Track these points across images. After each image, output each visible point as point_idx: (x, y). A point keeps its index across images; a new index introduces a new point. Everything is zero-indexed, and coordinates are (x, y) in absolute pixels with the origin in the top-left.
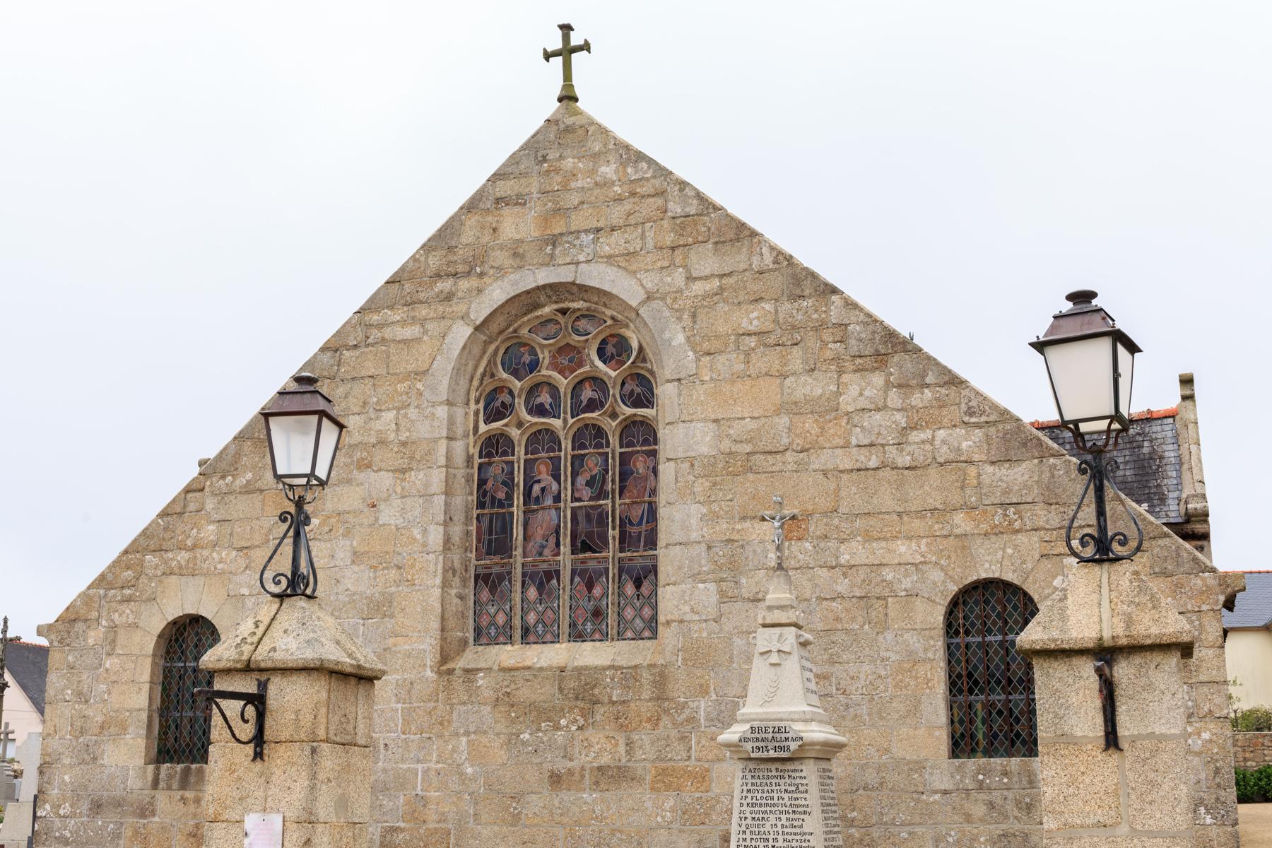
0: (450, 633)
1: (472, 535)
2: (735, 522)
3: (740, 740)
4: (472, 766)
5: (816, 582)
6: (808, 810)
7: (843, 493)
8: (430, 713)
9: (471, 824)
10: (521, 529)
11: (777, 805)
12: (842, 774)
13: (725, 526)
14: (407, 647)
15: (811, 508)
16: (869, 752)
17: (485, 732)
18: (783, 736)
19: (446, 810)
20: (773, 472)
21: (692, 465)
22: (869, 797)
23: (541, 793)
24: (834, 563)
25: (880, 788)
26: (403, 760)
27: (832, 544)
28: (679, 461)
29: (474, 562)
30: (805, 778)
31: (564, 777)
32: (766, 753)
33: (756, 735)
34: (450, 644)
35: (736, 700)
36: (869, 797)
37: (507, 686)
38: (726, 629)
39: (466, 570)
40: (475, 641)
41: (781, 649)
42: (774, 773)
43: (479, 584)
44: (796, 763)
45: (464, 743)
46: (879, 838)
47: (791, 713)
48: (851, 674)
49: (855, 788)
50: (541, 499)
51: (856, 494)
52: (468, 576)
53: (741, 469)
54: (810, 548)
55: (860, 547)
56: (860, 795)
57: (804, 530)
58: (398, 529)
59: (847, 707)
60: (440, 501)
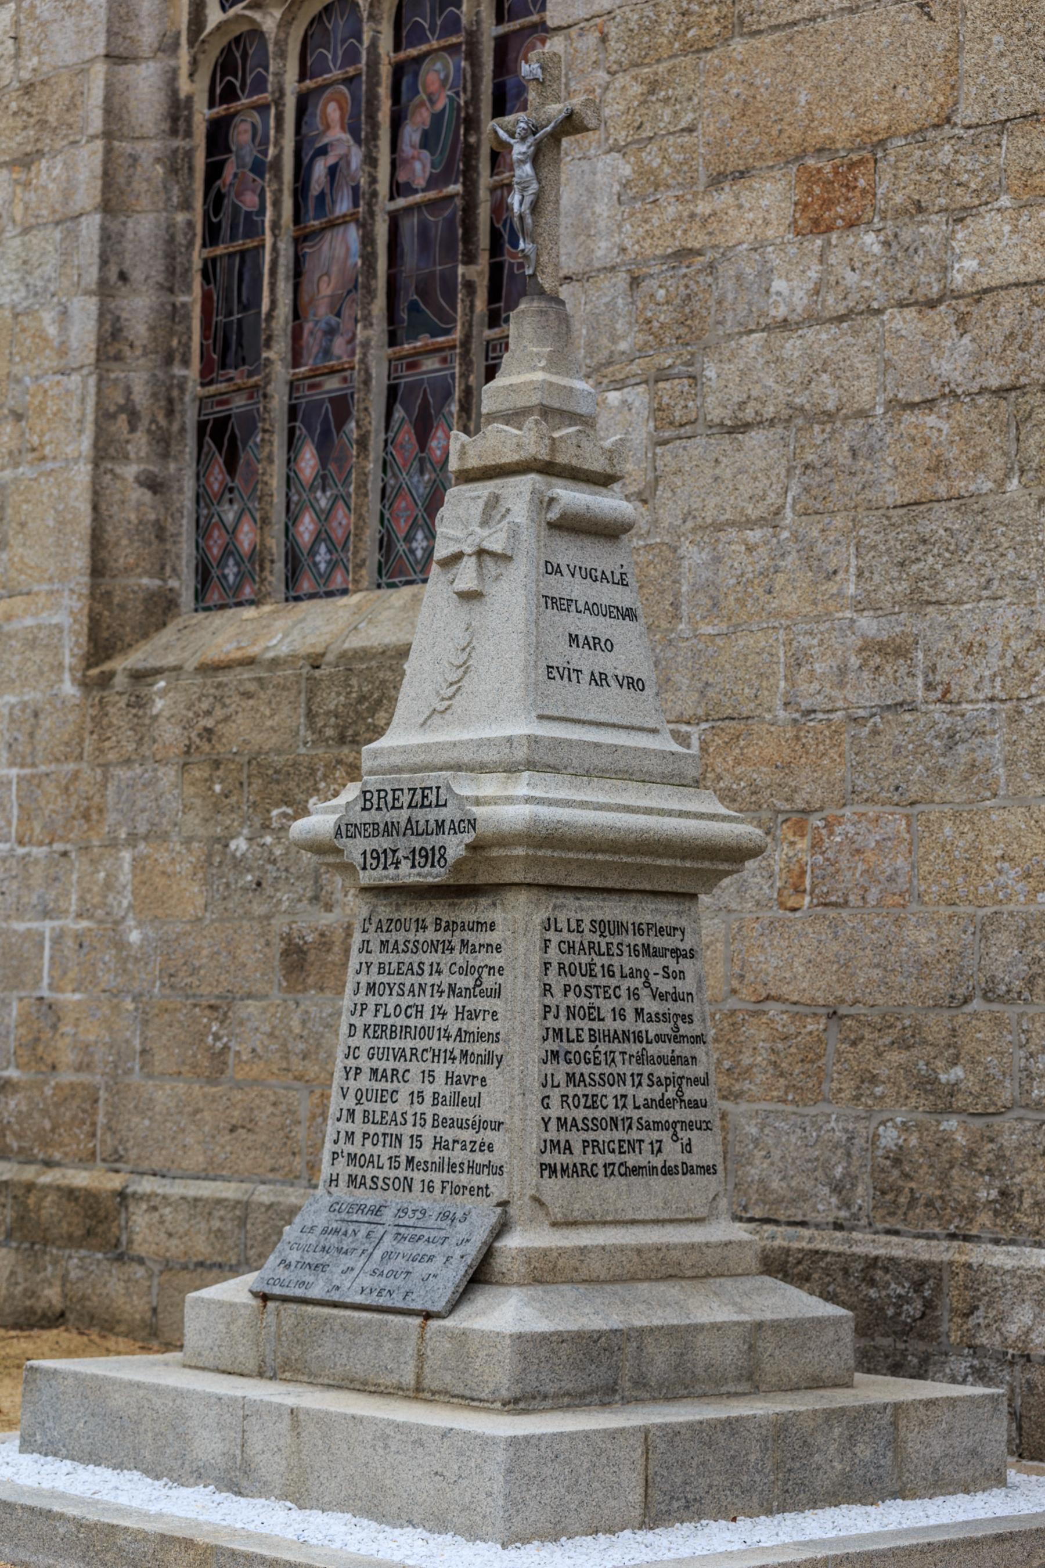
0: (122, 581)
1: (187, 317)
2: (695, 195)
3: (338, 833)
4: (140, 924)
5: (887, 353)
6: (498, 1049)
7: (967, 62)
8: (67, 789)
9: (136, 1078)
10: (284, 289)
11: (425, 1032)
12: (930, 949)
13: (671, 211)
14: (29, 622)
15: (883, 120)
16: (1002, 879)
17: (165, 837)
18: (433, 815)
19: (92, 1038)
20: (795, 23)
21: (604, 39)
22: (997, 1021)
23: (266, 996)
24: (935, 290)
25: (1026, 994)
26: (20, 912)
27: (933, 228)
28: (574, 32)
29: (194, 387)
30: (498, 948)
31: (311, 957)
32: (392, 871)
33: (374, 816)
34: (122, 607)
35: (684, 728)
36: (997, 1021)
37: (208, 713)
38: (667, 518)
39: (170, 413)
40: (196, 598)
41: (487, 545)
42: (430, 935)
43: (205, 449)
44: (484, 902)
45: (127, 867)
46: (1019, 1149)
47: (481, 743)
48: (967, 636)
49: (961, 992)
50: (328, 199)
51: (1002, 55)
52: (175, 427)
53: (716, 29)
54: (877, 249)
55: (1007, 228)
56: (975, 1014)
57: (864, 191)
58: (16, 316)
59: (952, 739)
60: (91, 227)
